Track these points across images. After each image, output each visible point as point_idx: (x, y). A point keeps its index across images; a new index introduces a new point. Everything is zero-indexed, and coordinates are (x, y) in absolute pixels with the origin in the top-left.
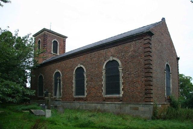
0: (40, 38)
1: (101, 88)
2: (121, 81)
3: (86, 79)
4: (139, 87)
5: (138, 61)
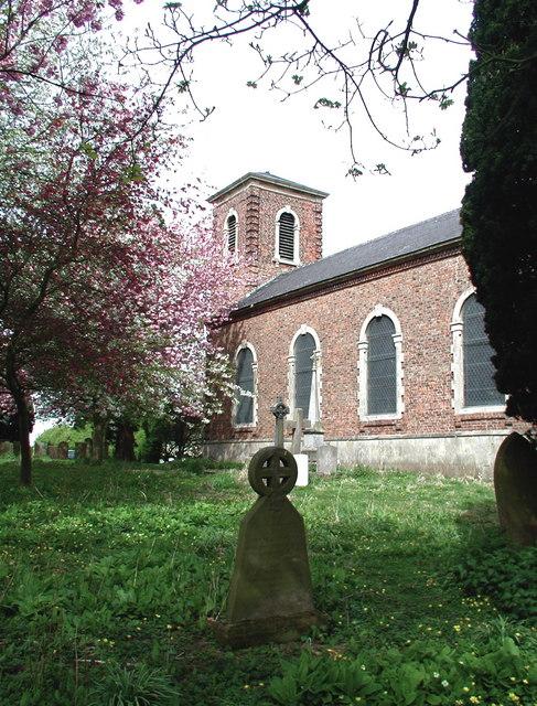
1: (449, 386)
3: (400, 357)
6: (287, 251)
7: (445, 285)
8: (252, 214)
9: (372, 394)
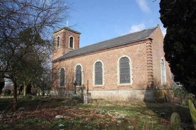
0: (59, 35)
2: (131, 73)
4: (144, 77)
5: (143, 59)
6: (71, 46)
7: (115, 55)
8: (64, 36)
9: (96, 80)
